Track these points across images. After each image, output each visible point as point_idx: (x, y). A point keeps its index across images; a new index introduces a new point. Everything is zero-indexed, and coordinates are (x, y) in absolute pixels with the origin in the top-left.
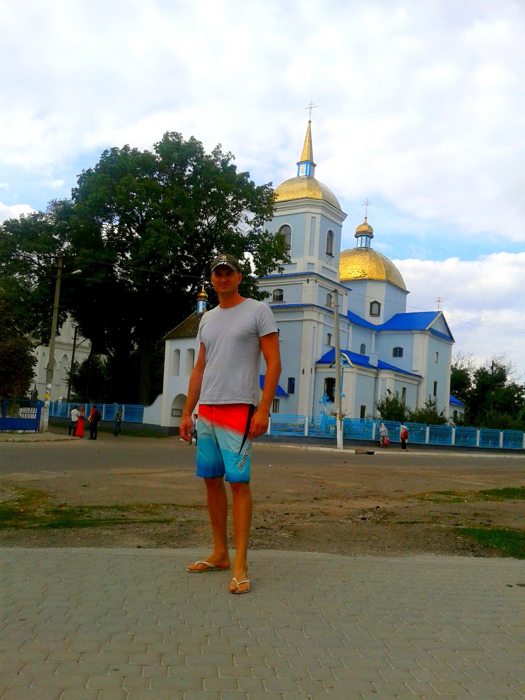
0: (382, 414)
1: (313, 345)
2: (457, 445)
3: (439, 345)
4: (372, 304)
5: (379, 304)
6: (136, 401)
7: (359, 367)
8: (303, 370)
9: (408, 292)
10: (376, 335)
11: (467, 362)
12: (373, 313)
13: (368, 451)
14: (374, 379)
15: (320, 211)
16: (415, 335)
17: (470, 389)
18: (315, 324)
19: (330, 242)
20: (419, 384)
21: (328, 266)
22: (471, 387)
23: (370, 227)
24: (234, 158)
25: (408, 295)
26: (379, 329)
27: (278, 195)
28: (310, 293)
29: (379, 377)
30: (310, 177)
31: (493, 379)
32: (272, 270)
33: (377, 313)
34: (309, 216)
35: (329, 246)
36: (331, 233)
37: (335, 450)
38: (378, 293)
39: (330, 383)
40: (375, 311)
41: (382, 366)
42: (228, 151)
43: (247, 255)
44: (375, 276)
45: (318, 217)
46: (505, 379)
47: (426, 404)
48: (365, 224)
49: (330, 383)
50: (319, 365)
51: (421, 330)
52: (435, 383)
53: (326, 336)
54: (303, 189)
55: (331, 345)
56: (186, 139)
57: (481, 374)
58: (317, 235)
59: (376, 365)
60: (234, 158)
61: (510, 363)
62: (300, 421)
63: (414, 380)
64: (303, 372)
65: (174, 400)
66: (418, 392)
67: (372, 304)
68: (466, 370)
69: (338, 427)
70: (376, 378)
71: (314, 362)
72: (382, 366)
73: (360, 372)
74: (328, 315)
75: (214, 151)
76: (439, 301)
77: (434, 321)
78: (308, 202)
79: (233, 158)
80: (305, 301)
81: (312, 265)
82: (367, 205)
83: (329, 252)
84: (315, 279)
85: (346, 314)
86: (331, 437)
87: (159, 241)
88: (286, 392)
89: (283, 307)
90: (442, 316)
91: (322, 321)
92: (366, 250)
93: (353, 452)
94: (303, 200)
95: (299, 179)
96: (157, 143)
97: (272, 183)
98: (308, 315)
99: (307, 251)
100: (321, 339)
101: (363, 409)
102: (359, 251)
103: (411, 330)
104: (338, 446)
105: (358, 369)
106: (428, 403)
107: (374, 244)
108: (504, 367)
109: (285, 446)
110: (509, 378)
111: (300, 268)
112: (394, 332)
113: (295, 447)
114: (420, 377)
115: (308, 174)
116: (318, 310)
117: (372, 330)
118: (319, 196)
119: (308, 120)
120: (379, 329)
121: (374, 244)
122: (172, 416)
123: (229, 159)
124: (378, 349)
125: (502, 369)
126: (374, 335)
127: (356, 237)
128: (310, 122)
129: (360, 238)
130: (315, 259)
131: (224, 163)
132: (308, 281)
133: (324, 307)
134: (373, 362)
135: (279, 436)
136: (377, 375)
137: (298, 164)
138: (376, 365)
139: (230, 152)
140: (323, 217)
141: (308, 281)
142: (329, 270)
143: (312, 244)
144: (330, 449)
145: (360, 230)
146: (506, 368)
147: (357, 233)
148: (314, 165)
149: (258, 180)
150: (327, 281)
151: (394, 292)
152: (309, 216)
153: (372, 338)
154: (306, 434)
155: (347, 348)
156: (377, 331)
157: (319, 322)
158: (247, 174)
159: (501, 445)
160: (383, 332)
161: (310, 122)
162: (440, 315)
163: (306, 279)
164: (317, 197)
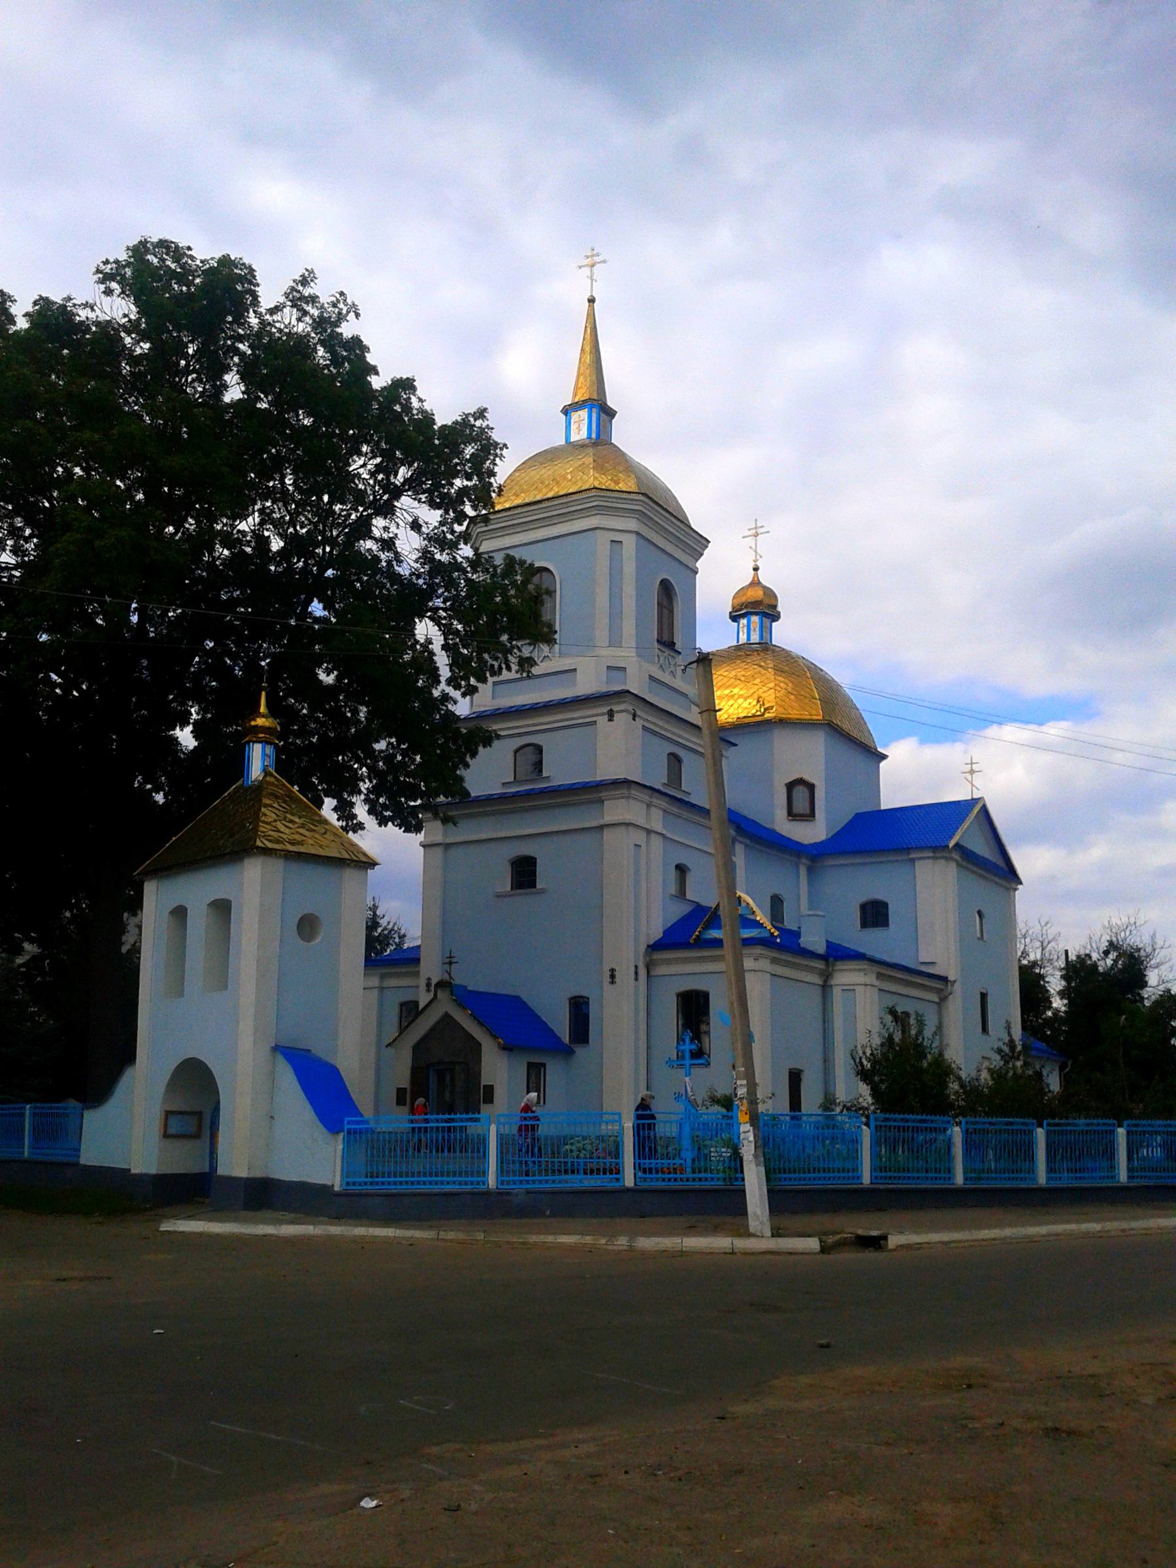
0: (875, 1093)
1: (637, 896)
2: (1135, 1183)
3: (984, 891)
4: (790, 786)
5: (811, 787)
6: (56, 1094)
7: (775, 954)
8: (613, 970)
9: (884, 757)
10: (810, 870)
11: (1038, 944)
12: (795, 811)
13: (860, 1232)
14: (818, 991)
15: (632, 524)
17: (1049, 1013)
18: (640, 838)
19: (666, 611)
21: (666, 678)
22: (1050, 1008)
23: (769, 593)
24: (357, 315)
25: (883, 764)
26: (814, 857)
27: (505, 446)
28: (617, 749)
29: (833, 982)
30: (600, 441)
31: (1108, 984)
32: (500, 668)
33: (808, 812)
34: (603, 539)
35: (665, 619)
36: (666, 588)
37: (742, 1244)
38: (807, 757)
39: (693, 1007)
40: (801, 806)
41: (836, 954)
42: (335, 290)
43: (424, 629)
44: (794, 714)
45: (629, 542)
46: (1144, 984)
47: (999, 1051)
48: (756, 583)
49: (693, 1007)
50: (658, 956)
51: (935, 849)
52: (984, 996)
53: (673, 874)
54: (582, 468)
55: (689, 896)
57: (1079, 971)
58: (629, 589)
59: (821, 949)
60: (357, 315)
61: (1153, 937)
62: (612, 1128)
64: (613, 976)
65: (168, 1085)
67: (790, 786)
68: (1034, 964)
69: (748, 1151)
70: (826, 988)
71: (643, 948)
72: (836, 954)
73: (780, 970)
74: (675, 810)
75: (293, 289)
77: (966, 825)
78: (600, 501)
79: (352, 315)
80: (607, 770)
81: (621, 673)
82: (756, 535)
83: (666, 638)
84: (630, 708)
86: (718, 1184)
87: (97, 543)
88: (566, 1039)
89: (543, 792)
90: (985, 811)
91: (657, 826)
92: (765, 647)
93: (813, 1244)
95: (573, 448)
96: (106, 262)
97: (485, 410)
98: (616, 810)
99: (602, 634)
100: (660, 880)
101: (795, 1078)
102: (740, 652)
103: (908, 850)
104: (753, 1225)
105: (774, 961)
106: (1006, 1049)
107: (783, 634)
108: (1139, 950)
109: (550, 1239)
110: (1152, 978)
111: (588, 682)
112: (858, 860)
113: (588, 1239)
114: (944, 979)
115: (594, 436)
116: (645, 796)
117: (799, 856)
118: (627, 484)
119: (588, 295)
120: (814, 857)
121: (783, 634)
122: (166, 1135)
123: (341, 318)
124: (824, 909)
125: (1131, 956)
126: (803, 871)
127: (734, 618)
128: (592, 301)
129: (744, 621)
130: (626, 655)
131: (326, 325)
132: (611, 715)
134: (814, 940)
135: (528, 1192)
136: (827, 976)
137: (566, 411)
138: (821, 949)
139: (342, 294)
140: (643, 543)
141: (611, 715)
143: (615, 614)
144: (722, 1242)
145: (743, 599)
146: (1142, 953)
147: (735, 609)
148: (611, 414)
149: (442, 403)
151: (847, 755)
152: (603, 539)
153: (798, 881)
154: (629, 1181)
156: (813, 861)
157: (649, 832)
158: (407, 385)
161: (592, 301)
162: (976, 810)
163: (606, 709)
164: (622, 486)
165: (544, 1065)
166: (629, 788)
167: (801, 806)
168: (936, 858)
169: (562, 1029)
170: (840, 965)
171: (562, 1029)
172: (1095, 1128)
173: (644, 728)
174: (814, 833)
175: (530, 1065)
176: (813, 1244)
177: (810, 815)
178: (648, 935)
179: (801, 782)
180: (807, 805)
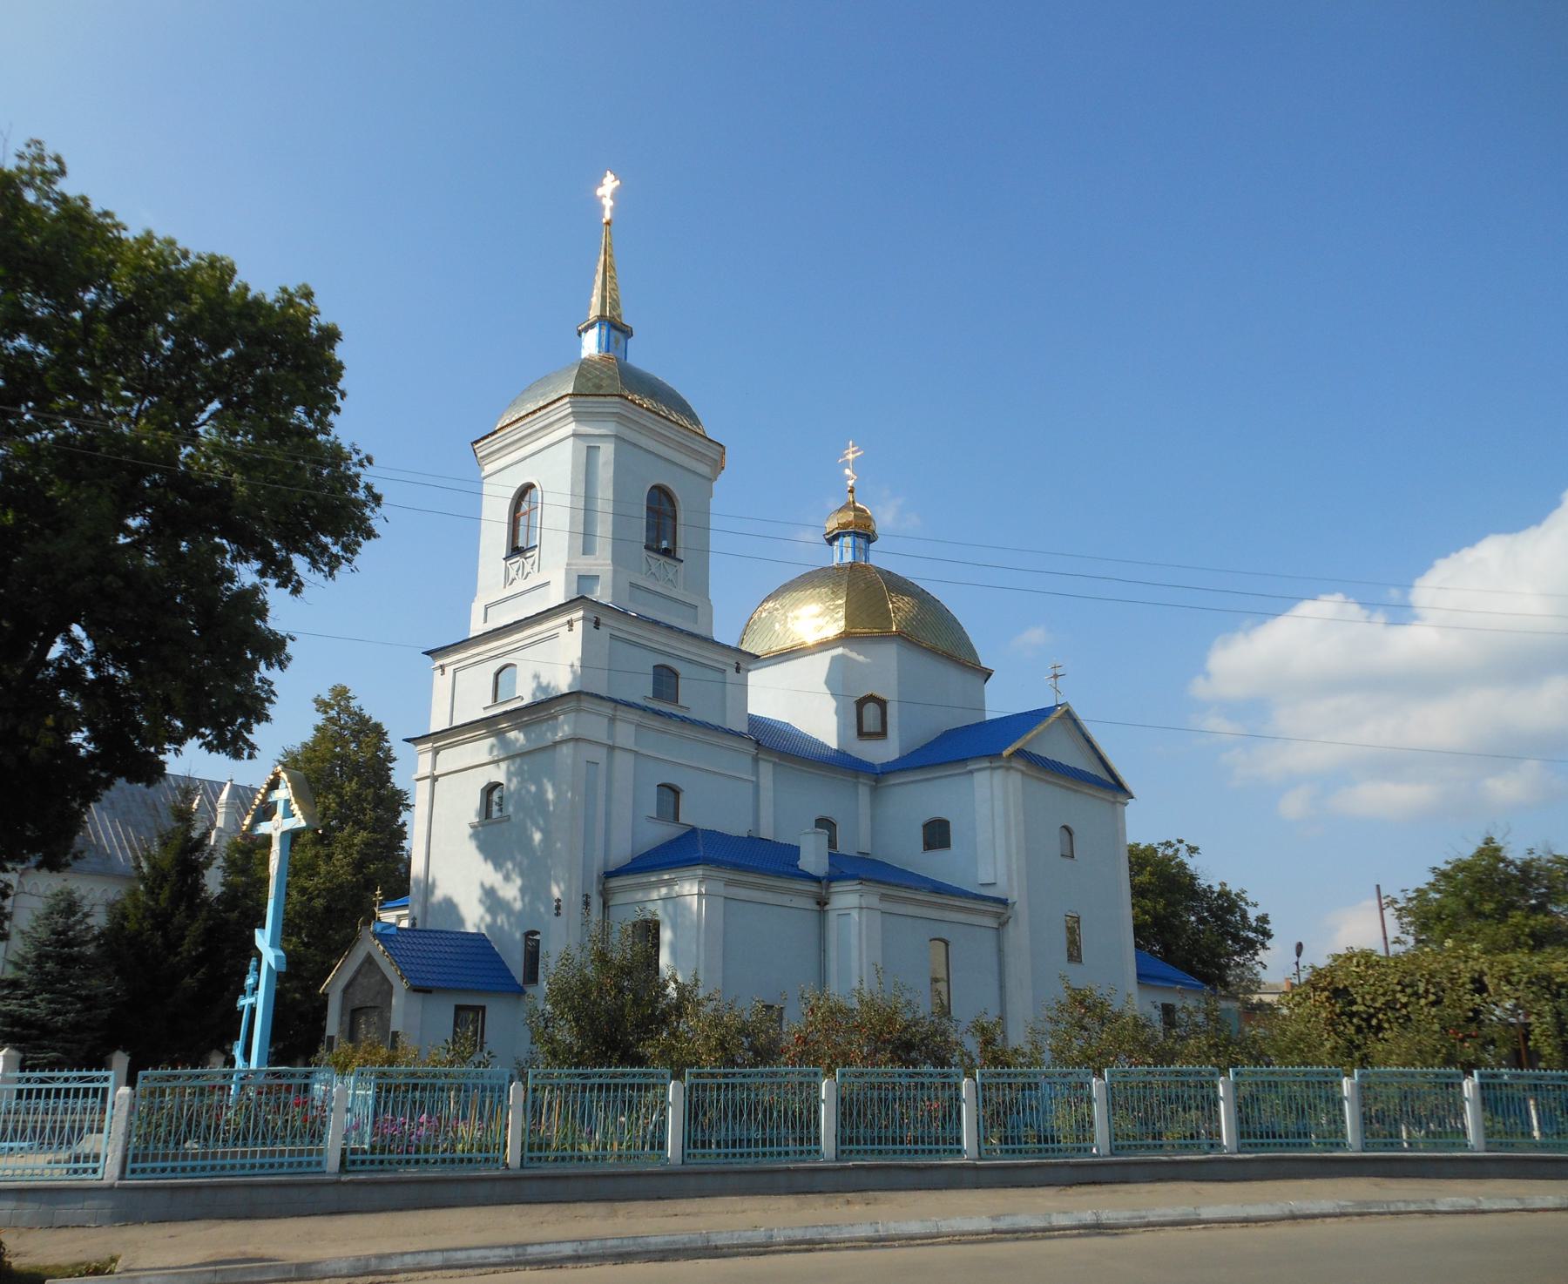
5: (882, 704)
9: (988, 674)
12: (865, 729)
16: (976, 775)
20: (1003, 924)
33: (879, 730)
40: (871, 722)
50: (615, 883)
63: (985, 913)
66: (1000, 951)
67: (861, 703)
88: (519, 978)
94: (531, 418)
103: (963, 761)
105: (883, 897)
112: (918, 776)
114: (1003, 902)
132: (570, 623)
136: (822, 903)
142: (684, 603)
150: (690, 640)
155: (758, 830)
157: (611, 748)
160: (893, 780)
165: (483, 1008)
166: (579, 700)
167: (871, 722)
168: (993, 769)
169: (518, 971)
170: (836, 887)
171: (518, 971)
173: (612, 636)
177: (882, 734)
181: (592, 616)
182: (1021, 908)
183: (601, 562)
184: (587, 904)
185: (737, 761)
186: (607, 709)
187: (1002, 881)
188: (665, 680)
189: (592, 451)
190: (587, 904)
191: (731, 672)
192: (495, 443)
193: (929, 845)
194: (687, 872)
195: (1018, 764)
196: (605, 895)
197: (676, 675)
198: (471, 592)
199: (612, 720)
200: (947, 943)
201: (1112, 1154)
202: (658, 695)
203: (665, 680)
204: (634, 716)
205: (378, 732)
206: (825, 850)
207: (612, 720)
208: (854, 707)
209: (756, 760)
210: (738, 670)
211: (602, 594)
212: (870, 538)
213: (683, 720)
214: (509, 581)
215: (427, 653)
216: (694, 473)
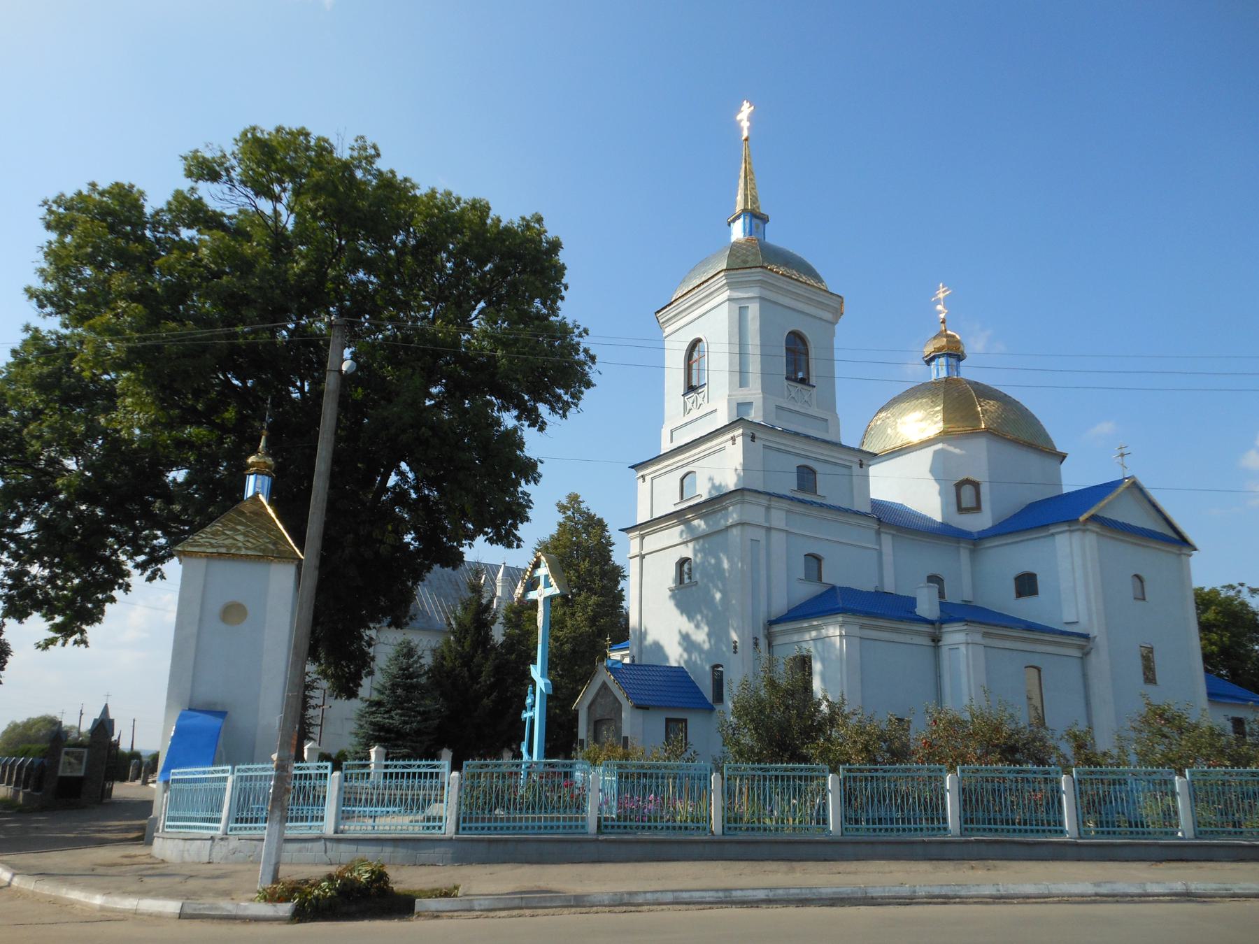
5: (976, 485)
9: (1063, 457)
12: (964, 506)
20: (1086, 654)
33: (964, 506)
50: (776, 628)
55: (824, 580)
56: (400, 177)
66: (1085, 676)
67: (959, 486)
73: (989, 642)
76: (1122, 455)
85: (868, 509)
105: (985, 635)
114: (1085, 637)
133: (790, 495)
134: (927, 606)
136: (936, 640)
148: (764, 219)
156: (974, 545)
159: (1185, 828)
160: (988, 544)
170: (947, 628)
171: (708, 694)
172: (401, 763)
173: (765, 447)
174: (981, 522)
175: (668, 720)
176: (171, 906)
177: (977, 508)
178: (769, 612)
179: (967, 482)
180: (974, 499)
181: (749, 432)
182: (1101, 640)
183: (754, 392)
184: (756, 644)
185: (864, 535)
186: (763, 500)
187: (1083, 620)
188: (806, 476)
189: (742, 310)
190: (756, 644)
191: (856, 468)
192: (671, 312)
193: (1020, 593)
194: (830, 619)
195: (1091, 526)
196: (770, 638)
197: (814, 472)
198: (660, 422)
199: (768, 508)
200: (1039, 670)
201: (1197, 838)
202: (801, 488)
203: (806, 476)
204: (785, 505)
205: (601, 525)
206: (937, 600)
207: (768, 508)
208: (953, 490)
209: (878, 533)
210: (861, 465)
211: (755, 415)
212: (960, 357)
213: (821, 505)
214: (687, 411)
215: (632, 467)
216: (820, 319)
